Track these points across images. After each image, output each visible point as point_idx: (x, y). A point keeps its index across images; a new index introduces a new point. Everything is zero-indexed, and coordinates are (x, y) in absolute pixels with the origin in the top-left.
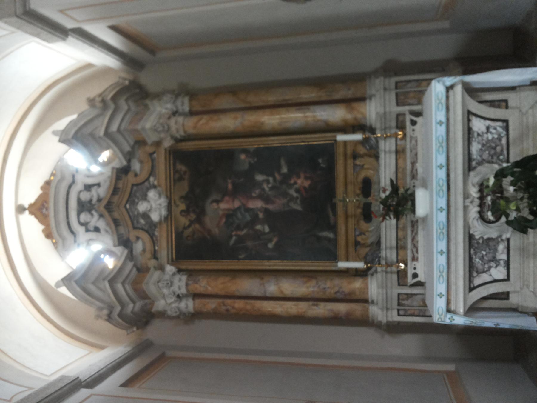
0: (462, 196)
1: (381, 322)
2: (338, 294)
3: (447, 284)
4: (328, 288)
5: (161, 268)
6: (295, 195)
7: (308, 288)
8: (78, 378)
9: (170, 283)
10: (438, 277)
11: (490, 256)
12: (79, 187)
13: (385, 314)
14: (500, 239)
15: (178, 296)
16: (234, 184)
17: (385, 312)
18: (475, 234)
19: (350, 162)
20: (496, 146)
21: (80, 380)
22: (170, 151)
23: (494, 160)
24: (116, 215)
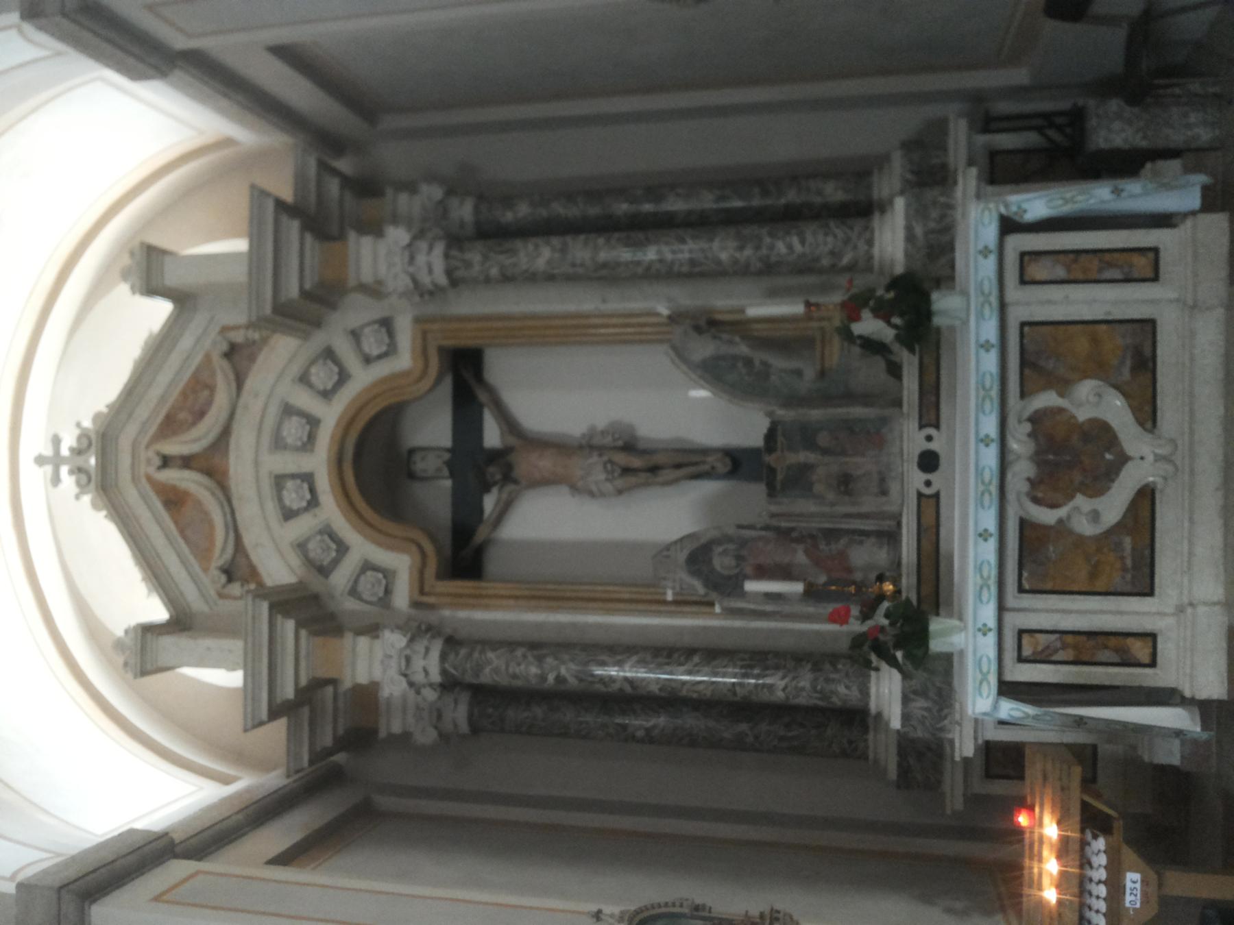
10: (978, 682)
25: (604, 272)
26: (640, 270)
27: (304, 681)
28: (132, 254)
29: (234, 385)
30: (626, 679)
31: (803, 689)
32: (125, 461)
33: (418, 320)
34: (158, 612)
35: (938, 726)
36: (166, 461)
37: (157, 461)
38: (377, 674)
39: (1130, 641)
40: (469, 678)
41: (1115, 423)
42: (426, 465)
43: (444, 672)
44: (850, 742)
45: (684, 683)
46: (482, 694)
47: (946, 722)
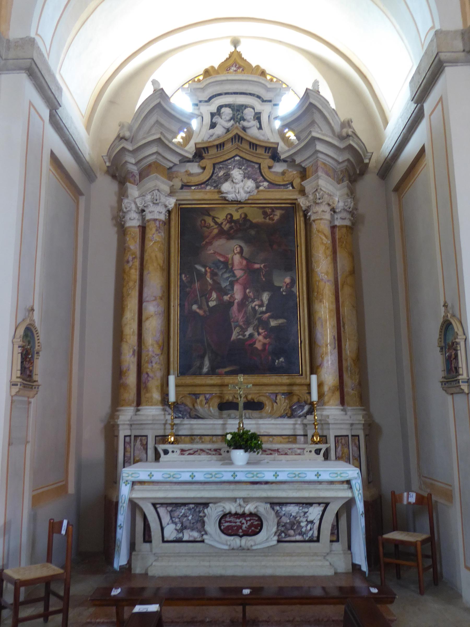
0: (246, 496)
1: (118, 418)
2: (146, 376)
3: (163, 481)
4: (152, 366)
5: (172, 193)
6: (247, 333)
7: (152, 345)
8: (61, 106)
9: (156, 202)
10: (294, 472)
11: (187, 524)
12: (259, 106)
13: (126, 423)
14: (203, 533)
15: (143, 211)
16: (260, 269)
17: (128, 422)
18: (209, 509)
19: (285, 389)
20: (294, 530)
21: (58, 109)
22: (295, 204)
23: (280, 528)
24: (228, 146)
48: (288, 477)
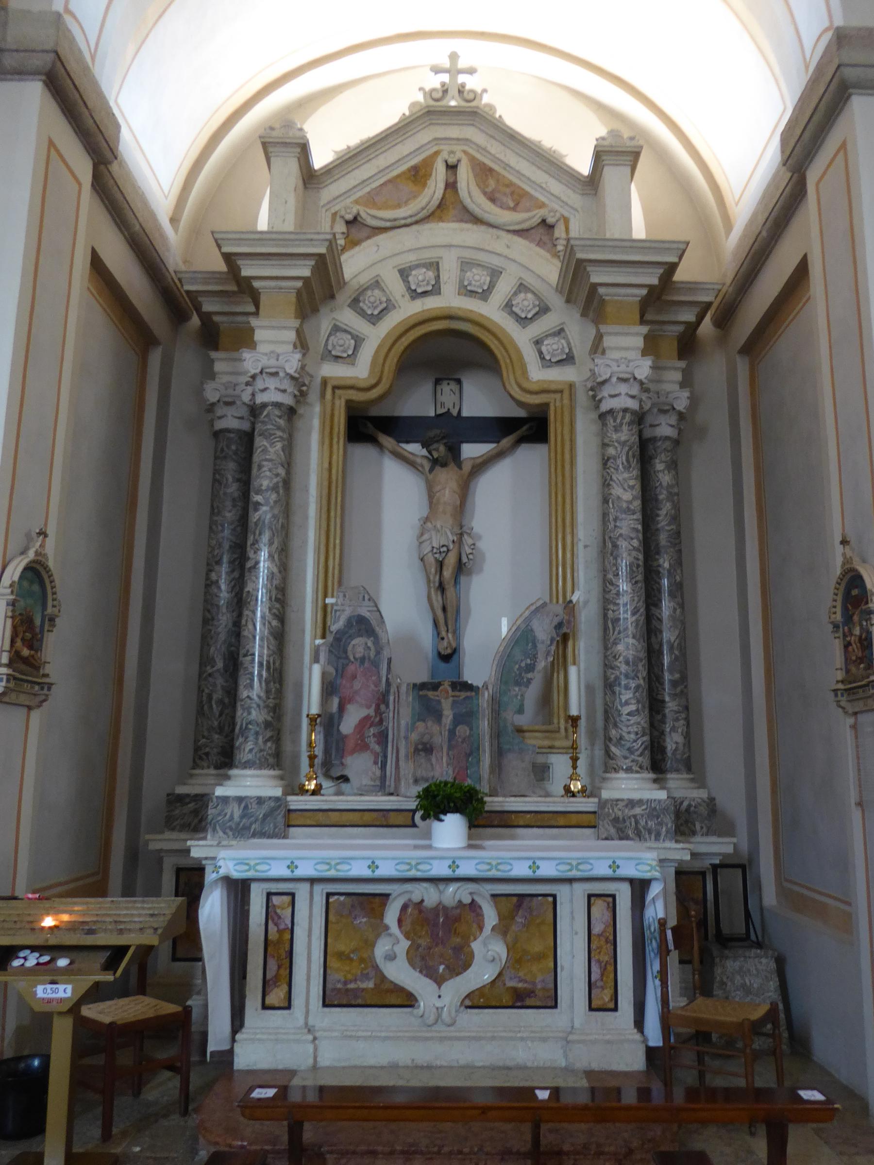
3: (397, 877)
25: (609, 545)
26: (610, 576)
27: (256, 284)
28: (632, 139)
29: (517, 227)
30: (257, 563)
31: (249, 713)
32: (454, 132)
33: (571, 386)
34: (320, 159)
35: (218, 827)
36: (452, 168)
37: (452, 160)
38: (262, 348)
39: (285, 987)
40: (259, 427)
41: (470, 973)
42: (448, 396)
43: (264, 405)
44: (207, 754)
45: (254, 612)
46: (247, 439)
47: (221, 834)
48: (397, 870)
